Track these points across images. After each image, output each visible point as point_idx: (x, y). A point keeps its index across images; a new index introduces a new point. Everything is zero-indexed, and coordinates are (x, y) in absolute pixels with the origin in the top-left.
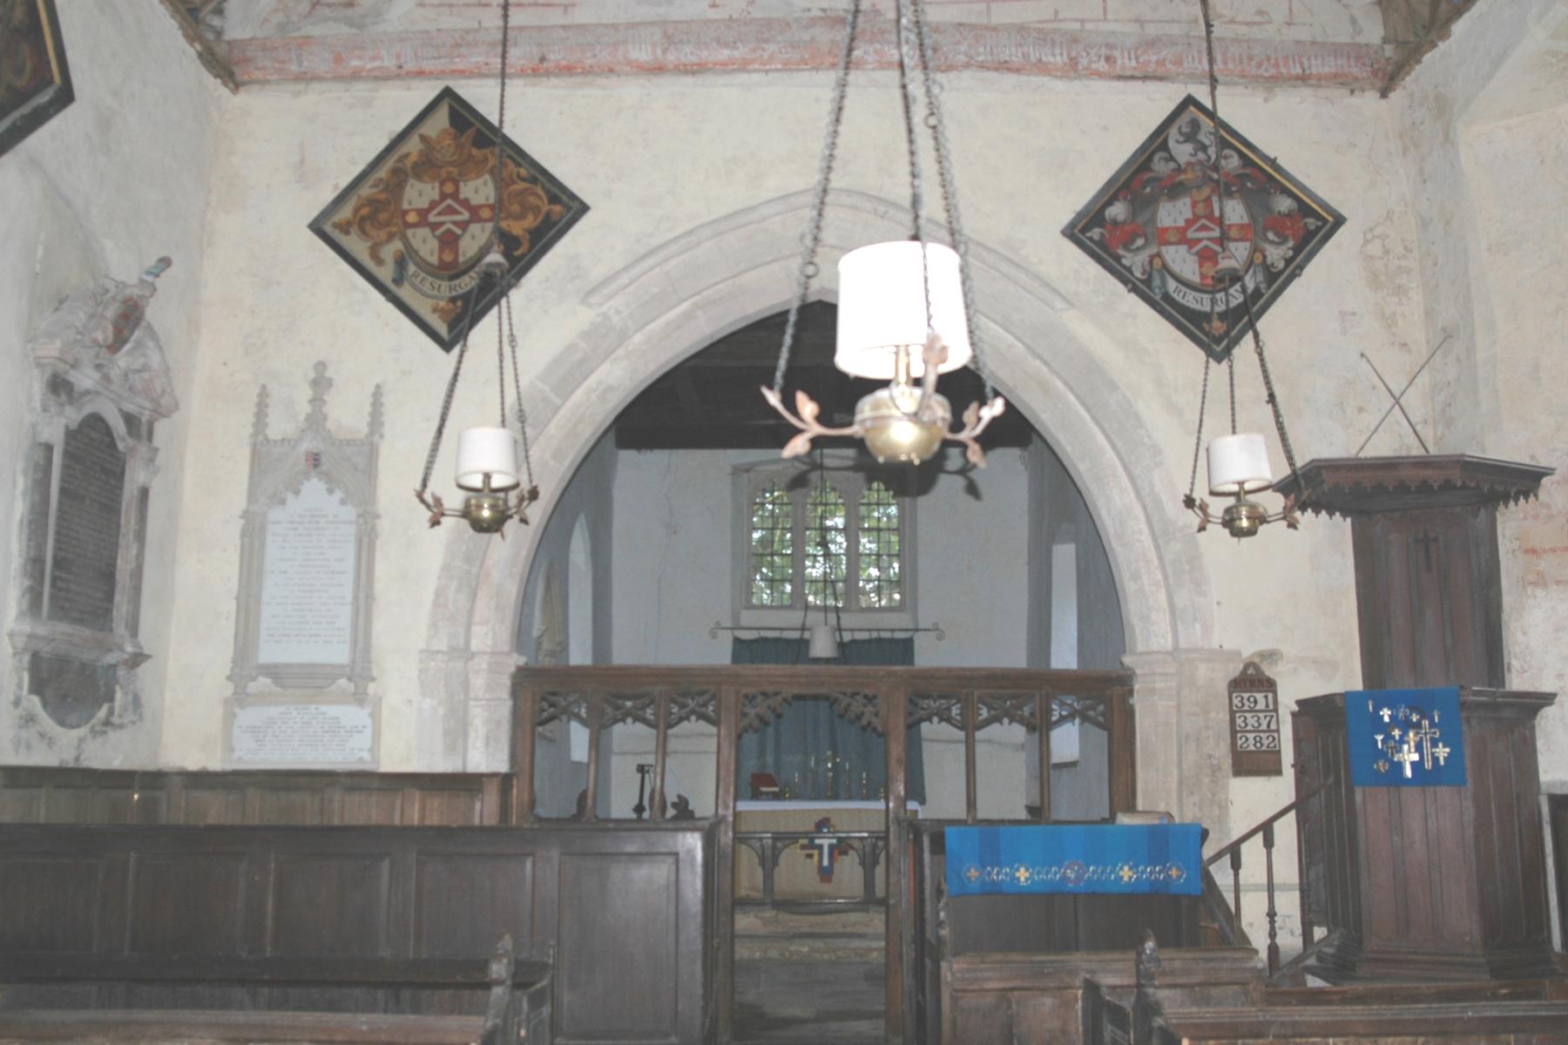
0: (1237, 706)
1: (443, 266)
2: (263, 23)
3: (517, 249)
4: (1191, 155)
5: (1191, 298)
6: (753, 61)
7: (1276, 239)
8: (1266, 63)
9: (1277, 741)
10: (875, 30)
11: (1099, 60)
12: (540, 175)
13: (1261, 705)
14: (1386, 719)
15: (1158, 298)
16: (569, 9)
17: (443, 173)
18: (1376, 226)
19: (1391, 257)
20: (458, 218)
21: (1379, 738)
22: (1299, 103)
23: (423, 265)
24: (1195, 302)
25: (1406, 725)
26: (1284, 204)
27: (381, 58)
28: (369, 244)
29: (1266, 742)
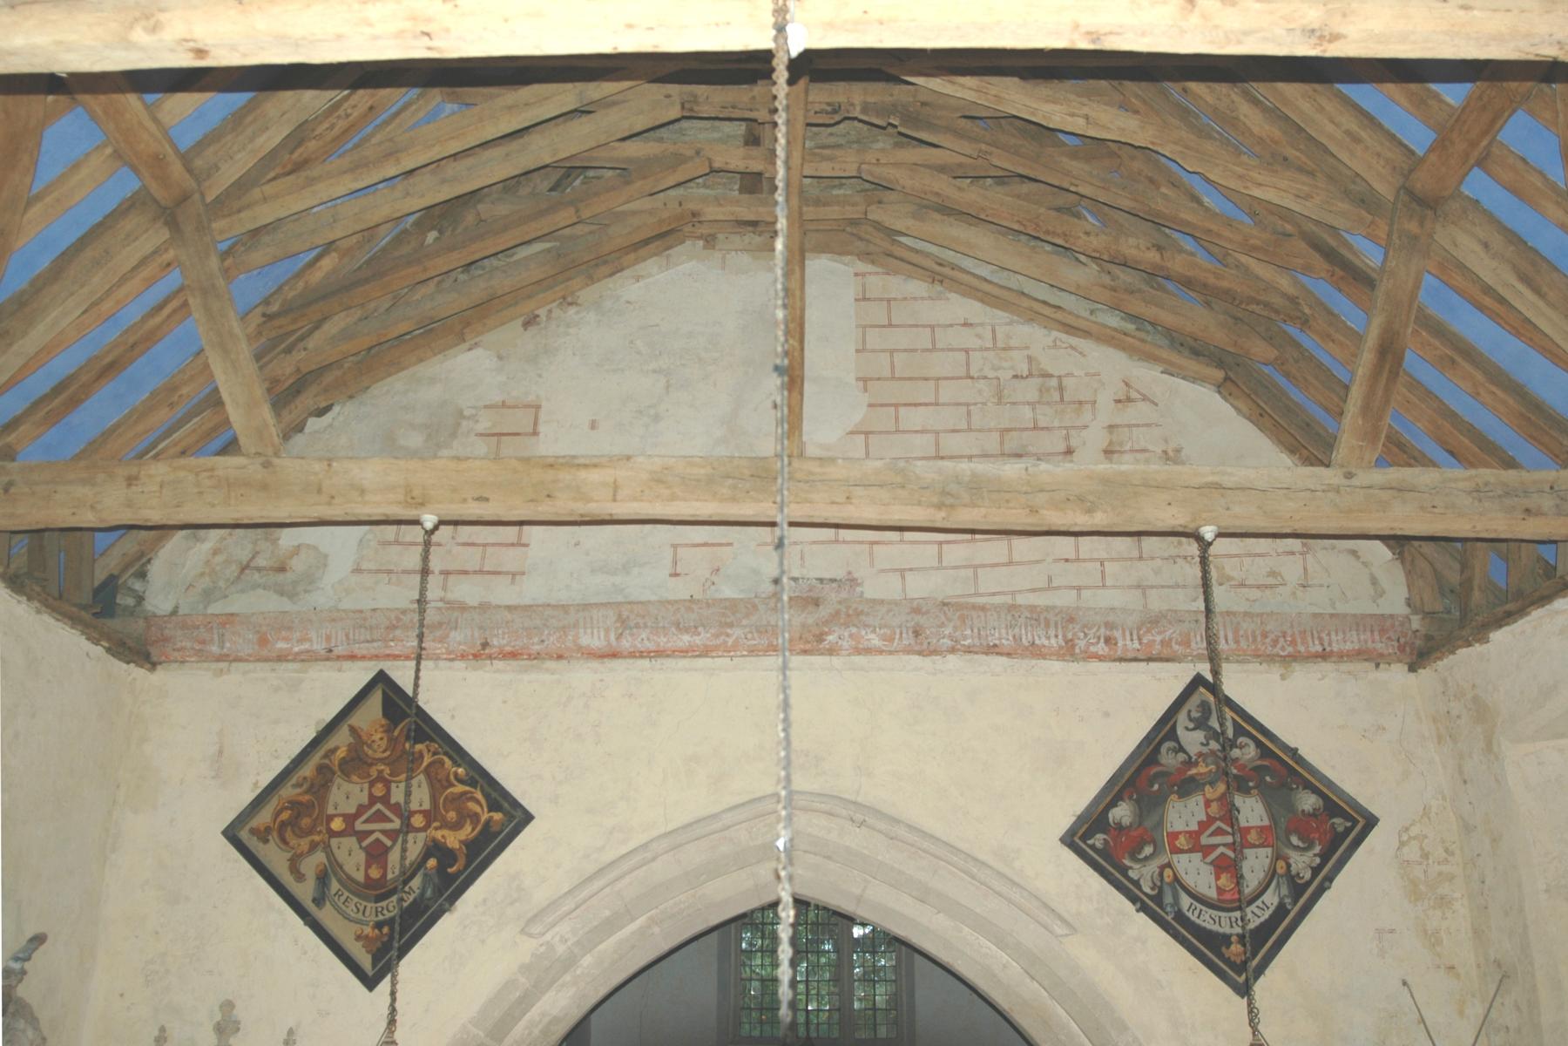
1: (370, 883)
2: (187, 589)
3: (451, 866)
4: (1202, 744)
5: (1207, 917)
6: (716, 648)
7: (1301, 845)
8: (1282, 640)
10: (851, 612)
11: (1098, 643)
12: (480, 777)
15: (1169, 918)
16: (518, 577)
17: (374, 772)
18: (1411, 825)
19: (1430, 861)
20: (388, 826)
22: (1319, 680)
23: (348, 882)
26: (1308, 802)
27: (310, 640)
28: (289, 855)
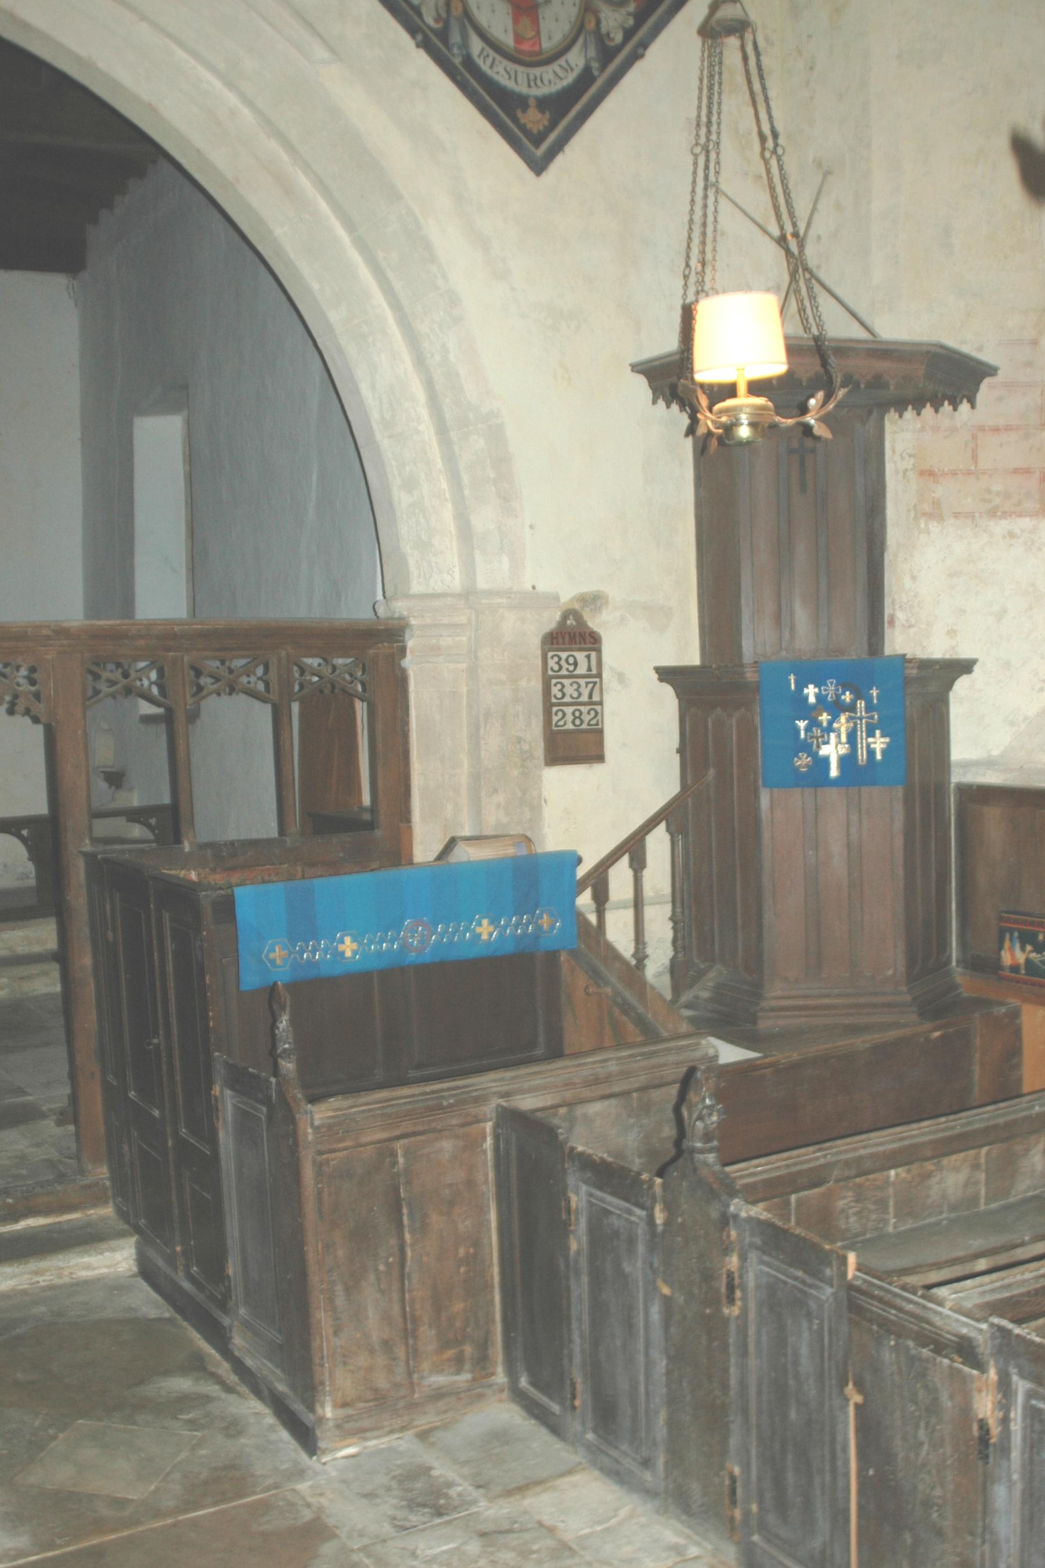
0: (552, 669)
5: (500, 69)
9: (599, 717)
13: (582, 670)
14: (812, 699)
15: (457, 61)
21: (802, 724)
24: (506, 76)
25: (837, 708)
29: (586, 718)
